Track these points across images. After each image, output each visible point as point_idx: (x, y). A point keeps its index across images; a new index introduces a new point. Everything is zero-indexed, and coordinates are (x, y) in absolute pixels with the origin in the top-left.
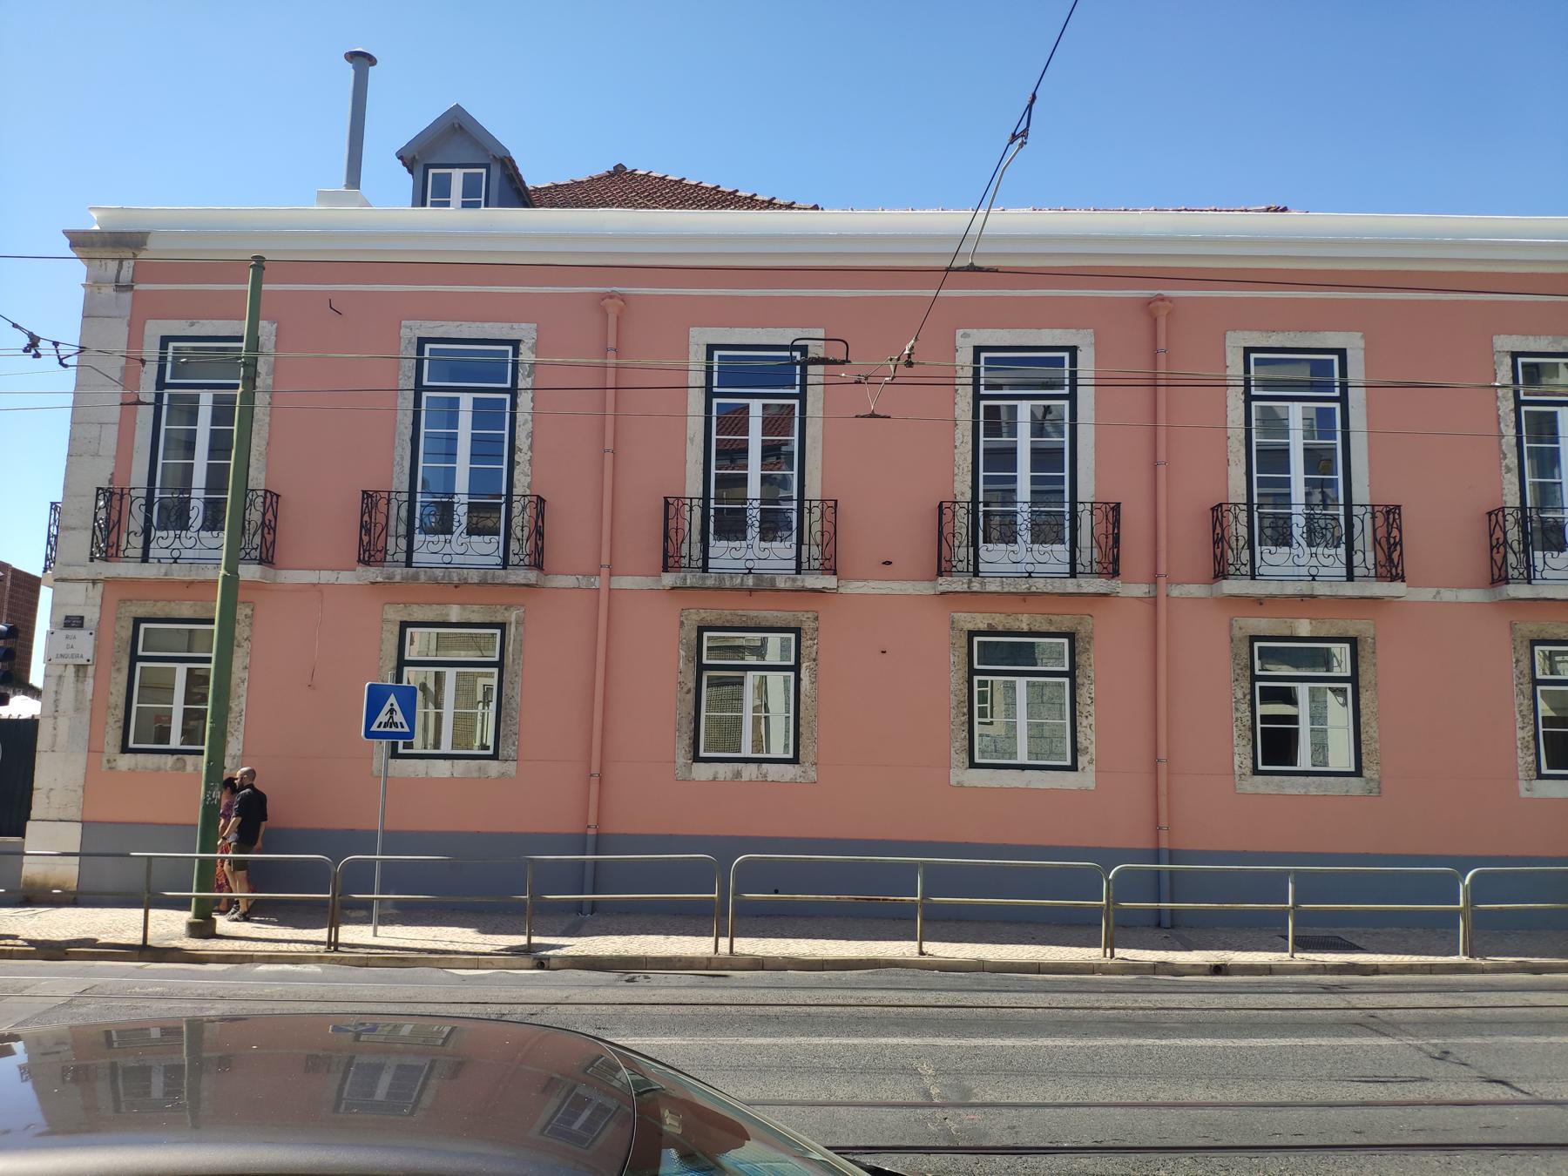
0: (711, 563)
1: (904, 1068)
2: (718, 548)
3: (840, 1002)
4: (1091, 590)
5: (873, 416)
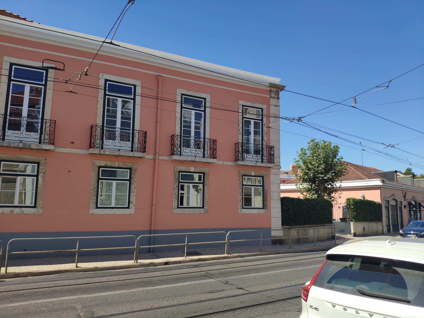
0: (6, 138)
1: (70, 307)
2: (9, 133)
3: (48, 286)
4: (137, 156)
5: (71, 92)
